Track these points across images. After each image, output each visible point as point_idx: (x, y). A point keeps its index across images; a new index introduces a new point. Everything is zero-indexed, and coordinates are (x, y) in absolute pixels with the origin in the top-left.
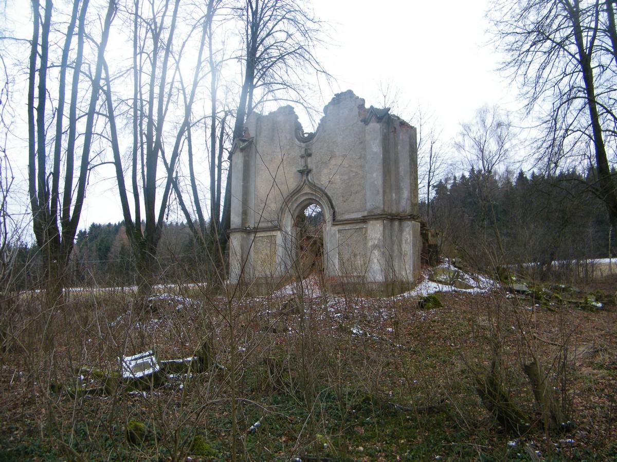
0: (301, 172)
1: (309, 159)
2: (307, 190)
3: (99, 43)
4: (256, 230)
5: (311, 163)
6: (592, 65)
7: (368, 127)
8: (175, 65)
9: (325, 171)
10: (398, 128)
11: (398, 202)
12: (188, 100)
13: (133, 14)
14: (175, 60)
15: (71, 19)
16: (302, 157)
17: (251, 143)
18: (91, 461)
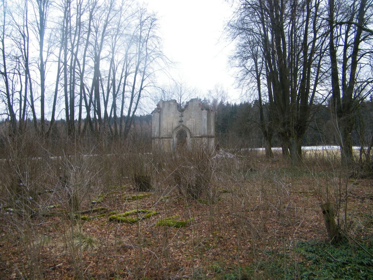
0: (180, 122)
1: (182, 118)
2: (181, 127)
3: (75, 73)
4: (162, 138)
5: (183, 119)
6: (260, 79)
7: (203, 111)
8: (370, 84)
9: (188, 122)
10: (211, 112)
11: (210, 133)
12: (106, 99)
13: (8, 73)
14: (366, 85)
15: (267, 89)
16: (180, 117)
17: (161, 110)
18: (212, 279)
